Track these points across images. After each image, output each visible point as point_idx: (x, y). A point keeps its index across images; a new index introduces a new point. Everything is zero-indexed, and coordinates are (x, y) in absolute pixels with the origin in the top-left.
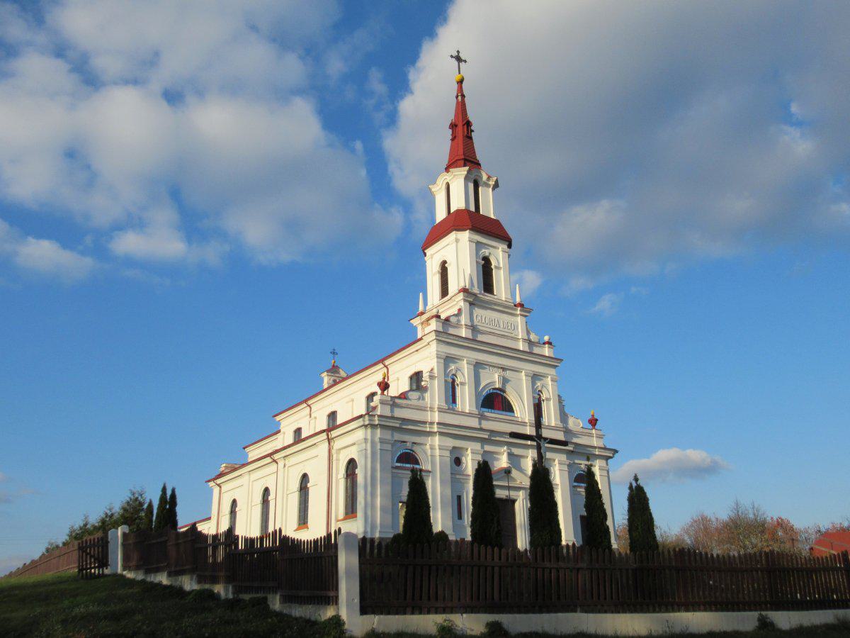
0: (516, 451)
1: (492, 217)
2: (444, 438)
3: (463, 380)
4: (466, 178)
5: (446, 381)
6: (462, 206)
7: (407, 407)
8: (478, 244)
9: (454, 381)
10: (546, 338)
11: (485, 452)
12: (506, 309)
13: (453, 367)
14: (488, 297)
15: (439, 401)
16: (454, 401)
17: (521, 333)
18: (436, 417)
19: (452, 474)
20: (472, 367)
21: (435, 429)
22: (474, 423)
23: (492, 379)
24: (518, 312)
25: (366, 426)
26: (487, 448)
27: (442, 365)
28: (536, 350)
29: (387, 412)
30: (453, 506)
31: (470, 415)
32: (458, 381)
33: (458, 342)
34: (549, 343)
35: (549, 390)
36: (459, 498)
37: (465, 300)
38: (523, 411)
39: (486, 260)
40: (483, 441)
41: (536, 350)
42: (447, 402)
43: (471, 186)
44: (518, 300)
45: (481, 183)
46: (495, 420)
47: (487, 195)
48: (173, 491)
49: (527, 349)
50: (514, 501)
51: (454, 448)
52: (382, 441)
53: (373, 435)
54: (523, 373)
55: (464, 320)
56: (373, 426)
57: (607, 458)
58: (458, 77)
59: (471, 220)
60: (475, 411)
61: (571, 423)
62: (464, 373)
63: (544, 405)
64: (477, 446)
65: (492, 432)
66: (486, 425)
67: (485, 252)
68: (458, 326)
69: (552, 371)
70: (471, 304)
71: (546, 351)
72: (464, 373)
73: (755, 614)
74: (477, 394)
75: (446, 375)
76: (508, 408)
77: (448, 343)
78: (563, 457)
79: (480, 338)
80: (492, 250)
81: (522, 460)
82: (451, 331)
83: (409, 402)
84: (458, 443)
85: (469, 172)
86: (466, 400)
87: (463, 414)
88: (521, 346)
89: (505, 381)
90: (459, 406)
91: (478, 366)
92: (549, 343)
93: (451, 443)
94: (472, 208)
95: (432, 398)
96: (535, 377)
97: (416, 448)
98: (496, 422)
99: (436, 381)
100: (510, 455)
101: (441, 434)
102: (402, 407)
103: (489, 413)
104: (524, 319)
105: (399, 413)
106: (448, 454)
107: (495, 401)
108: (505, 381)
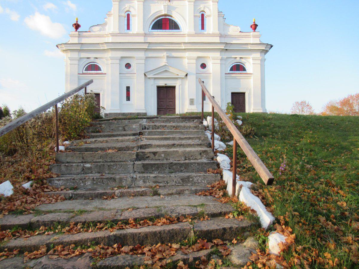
57: (266, 52)
66: (150, 40)
76: (174, 26)
78: (218, 55)
108: (169, 8)
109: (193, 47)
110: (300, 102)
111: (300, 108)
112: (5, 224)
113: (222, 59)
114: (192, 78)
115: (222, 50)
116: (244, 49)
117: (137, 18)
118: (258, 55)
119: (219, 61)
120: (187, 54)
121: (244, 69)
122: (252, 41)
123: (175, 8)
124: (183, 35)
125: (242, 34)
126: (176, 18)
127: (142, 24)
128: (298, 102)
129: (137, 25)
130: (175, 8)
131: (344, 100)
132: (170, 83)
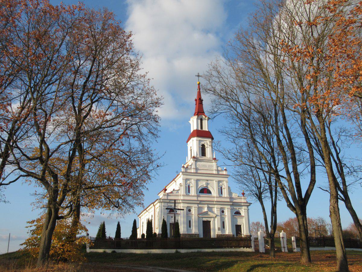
0: (210, 206)
1: (207, 130)
2: (184, 204)
3: (192, 186)
4: (197, 119)
5: (218, 188)
6: (195, 128)
7: (172, 195)
8: (200, 141)
9: (221, 188)
10: (225, 168)
11: (199, 207)
12: (209, 161)
13: (221, 184)
14: (204, 158)
15: (183, 193)
16: (222, 194)
17: (215, 168)
18: (182, 198)
19: (187, 214)
20: (195, 181)
21: (181, 201)
22: (195, 198)
23: (202, 184)
24: (213, 161)
25: (159, 202)
26: (200, 206)
27: (184, 182)
28: (189, 171)
29: (166, 198)
30: (187, 224)
31: (194, 196)
32: (223, 187)
33: (191, 174)
34: (226, 170)
35: (225, 185)
36: (190, 222)
37: (193, 160)
38: (214, 192)
39: (203, 146)
40: (198, 204)
41: (220, 173)
42: (219, 194)
43: (199, 121)
44: (214, 157)
45: (203, 119)
46: (203, 197)
47: (205, 123)
48: (29, 222)
49: (216, 173)
50: (210, 221)
51: (221, 208)
52: (164, 206)
53: (161, 205)
54: (215, 181)
55: (193, 166)
56: (161, 202)
57: (248, 206)
58: (198, 83)
59: (200, 134)
60: (196, 194)
61: (234, 195)
62: (193, 183)
63: (223, 190)
64: (196, 206)
65: (201, 201)
66: (200, 199)
67: (203, 143)
68: (191, 169)
69: (226, 179)
70: (196, 161)
71: (224, 173)
72: (193, 183)
73: (175, 250)
74: (197, 189)
75: (186, 184)
76: (209, 192)
77: (187, 175)
78: (229, 207)
79: (199, 172)
80: (205, 142)
81: (213, 209)
82: (189, 171)
83: (173, 194)
84: (222, 206)
85: (198, 117)
86: (193, 191)
87: (225, 198)
88: (215, 172)
89: (207, 184)
90: (223, 196)
91: (197, 181)
92: (226, 170)
93: (186, 205)
94: (200, 129)
95: (181, 192)
96: (219, 182)
97: (239, 210)
98: (204, 197)
99: (182, 187)
100: (208, 207)
101: (183, 203)
102: (170, 196)
103: (202, 195)
104: (216, 163)
105: (170, 198)
106: (219, 210)
107: (205, 191)
108: (207, 184)
109: (218, 203)
110: (255, 222)
111: (256, 228)
112: (242, 251)
113: (231, 209)
114: (219, 217)
115: (230, 205)
116: (239, 205)
117: (193, 188)
118: (246, 208)
119: (230, 210)
120: (216, 206)
121: (240, 214)
122: (243, 201)
123: (209, 184)
124: (214, 197)
125: (239, 197)
126: (210, 189)
127: (195, 191)
128: (254, 223)
129: (193, 191)
130: (209, 184)
131: (287, 222)
132: (209, 219)
